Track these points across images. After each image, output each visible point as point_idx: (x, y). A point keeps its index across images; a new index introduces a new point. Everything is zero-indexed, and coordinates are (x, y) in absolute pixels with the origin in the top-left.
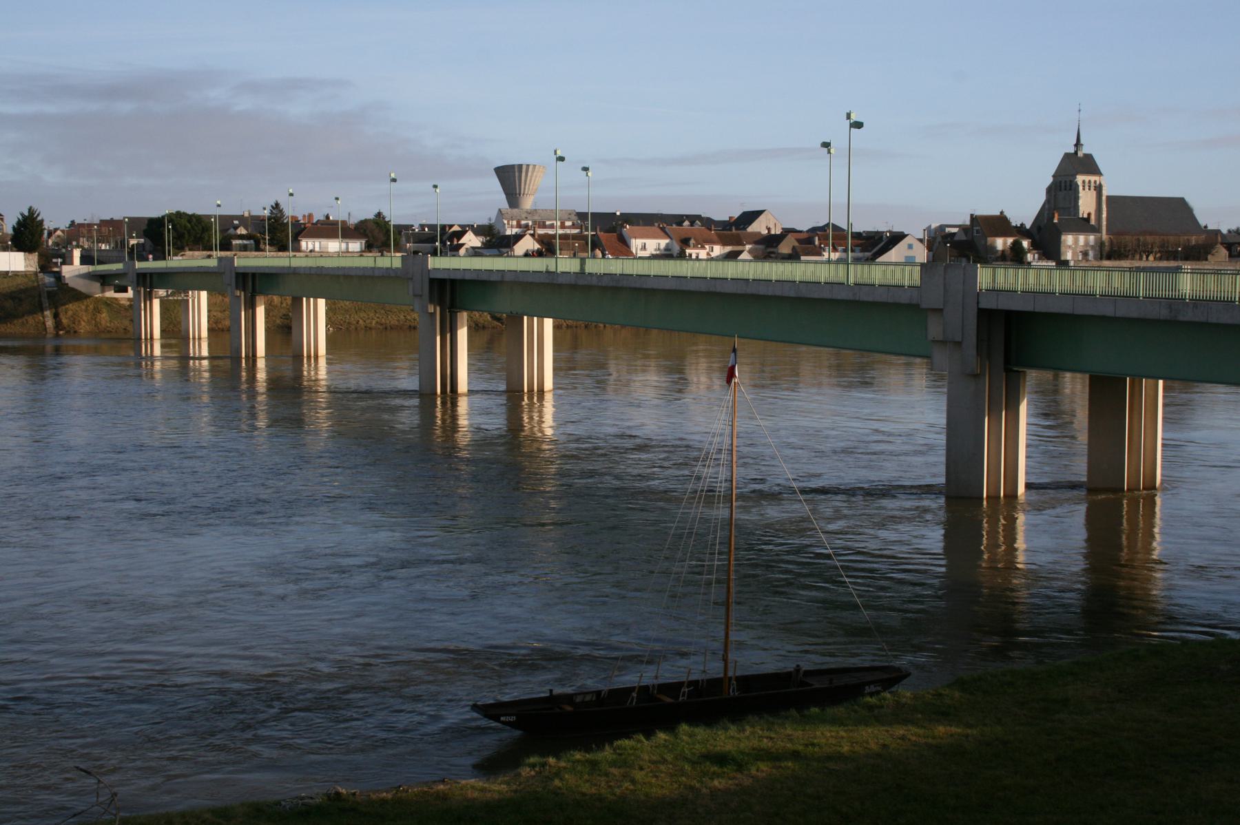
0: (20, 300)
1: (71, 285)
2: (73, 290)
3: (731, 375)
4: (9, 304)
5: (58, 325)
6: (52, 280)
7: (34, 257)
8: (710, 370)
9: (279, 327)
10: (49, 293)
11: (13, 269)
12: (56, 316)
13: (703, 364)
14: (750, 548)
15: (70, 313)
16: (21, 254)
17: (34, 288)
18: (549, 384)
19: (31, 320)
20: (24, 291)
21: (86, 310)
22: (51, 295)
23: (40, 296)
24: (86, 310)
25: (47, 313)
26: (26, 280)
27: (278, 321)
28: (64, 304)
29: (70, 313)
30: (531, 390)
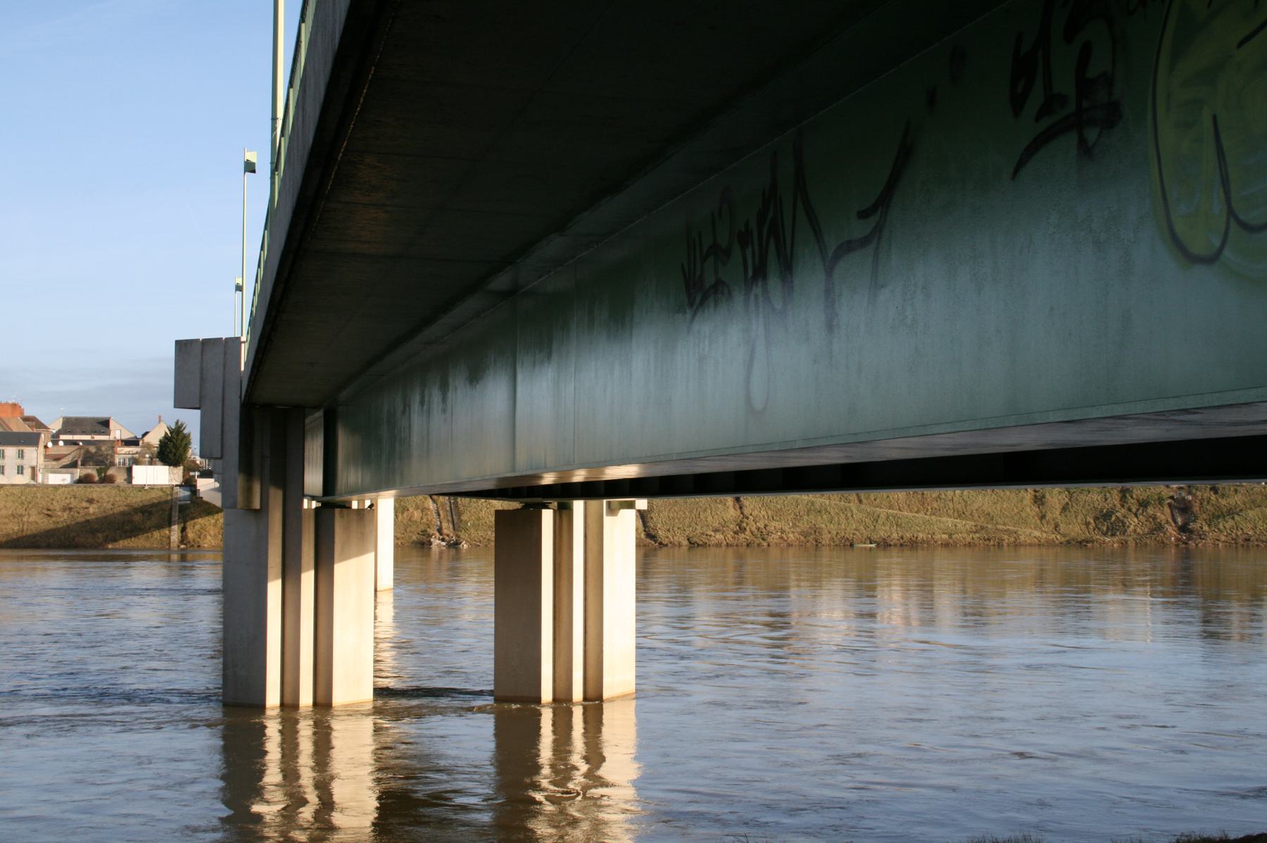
0: (151, 513)
1: (205, 499)
2: (207, 503)
3: (1167, 623)
4: (138, 518)
5: (183, 539)
6: (188, 493)
7: (179, 471)
8: (906, 589)
9: (414, 542)
10: (181, 506)
11: (151, 482)
12: (183, 530)
13: (897, 581)
14: (511, 293)
15: (198, 527)
16: (167, 467)
17: (167, 502)
18: (620, 675)
19: (156, 534)
20: (153, 505)
21: (215, 525)
22: (183, 509)
23: (171, 509)
24: (215, 525)
25: (175, 528)
26: (161, 493)
27: (414, 538)
28: (193, 518)
29: (198, 527)
30: (562, 701)
